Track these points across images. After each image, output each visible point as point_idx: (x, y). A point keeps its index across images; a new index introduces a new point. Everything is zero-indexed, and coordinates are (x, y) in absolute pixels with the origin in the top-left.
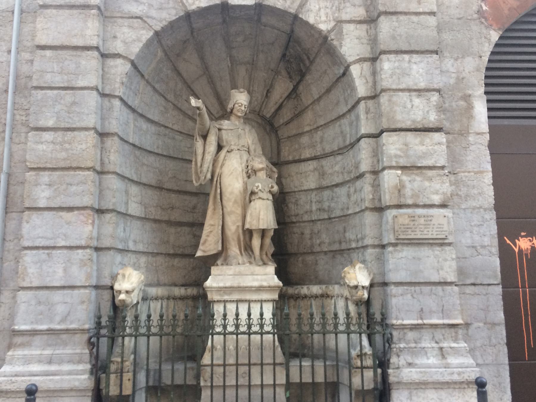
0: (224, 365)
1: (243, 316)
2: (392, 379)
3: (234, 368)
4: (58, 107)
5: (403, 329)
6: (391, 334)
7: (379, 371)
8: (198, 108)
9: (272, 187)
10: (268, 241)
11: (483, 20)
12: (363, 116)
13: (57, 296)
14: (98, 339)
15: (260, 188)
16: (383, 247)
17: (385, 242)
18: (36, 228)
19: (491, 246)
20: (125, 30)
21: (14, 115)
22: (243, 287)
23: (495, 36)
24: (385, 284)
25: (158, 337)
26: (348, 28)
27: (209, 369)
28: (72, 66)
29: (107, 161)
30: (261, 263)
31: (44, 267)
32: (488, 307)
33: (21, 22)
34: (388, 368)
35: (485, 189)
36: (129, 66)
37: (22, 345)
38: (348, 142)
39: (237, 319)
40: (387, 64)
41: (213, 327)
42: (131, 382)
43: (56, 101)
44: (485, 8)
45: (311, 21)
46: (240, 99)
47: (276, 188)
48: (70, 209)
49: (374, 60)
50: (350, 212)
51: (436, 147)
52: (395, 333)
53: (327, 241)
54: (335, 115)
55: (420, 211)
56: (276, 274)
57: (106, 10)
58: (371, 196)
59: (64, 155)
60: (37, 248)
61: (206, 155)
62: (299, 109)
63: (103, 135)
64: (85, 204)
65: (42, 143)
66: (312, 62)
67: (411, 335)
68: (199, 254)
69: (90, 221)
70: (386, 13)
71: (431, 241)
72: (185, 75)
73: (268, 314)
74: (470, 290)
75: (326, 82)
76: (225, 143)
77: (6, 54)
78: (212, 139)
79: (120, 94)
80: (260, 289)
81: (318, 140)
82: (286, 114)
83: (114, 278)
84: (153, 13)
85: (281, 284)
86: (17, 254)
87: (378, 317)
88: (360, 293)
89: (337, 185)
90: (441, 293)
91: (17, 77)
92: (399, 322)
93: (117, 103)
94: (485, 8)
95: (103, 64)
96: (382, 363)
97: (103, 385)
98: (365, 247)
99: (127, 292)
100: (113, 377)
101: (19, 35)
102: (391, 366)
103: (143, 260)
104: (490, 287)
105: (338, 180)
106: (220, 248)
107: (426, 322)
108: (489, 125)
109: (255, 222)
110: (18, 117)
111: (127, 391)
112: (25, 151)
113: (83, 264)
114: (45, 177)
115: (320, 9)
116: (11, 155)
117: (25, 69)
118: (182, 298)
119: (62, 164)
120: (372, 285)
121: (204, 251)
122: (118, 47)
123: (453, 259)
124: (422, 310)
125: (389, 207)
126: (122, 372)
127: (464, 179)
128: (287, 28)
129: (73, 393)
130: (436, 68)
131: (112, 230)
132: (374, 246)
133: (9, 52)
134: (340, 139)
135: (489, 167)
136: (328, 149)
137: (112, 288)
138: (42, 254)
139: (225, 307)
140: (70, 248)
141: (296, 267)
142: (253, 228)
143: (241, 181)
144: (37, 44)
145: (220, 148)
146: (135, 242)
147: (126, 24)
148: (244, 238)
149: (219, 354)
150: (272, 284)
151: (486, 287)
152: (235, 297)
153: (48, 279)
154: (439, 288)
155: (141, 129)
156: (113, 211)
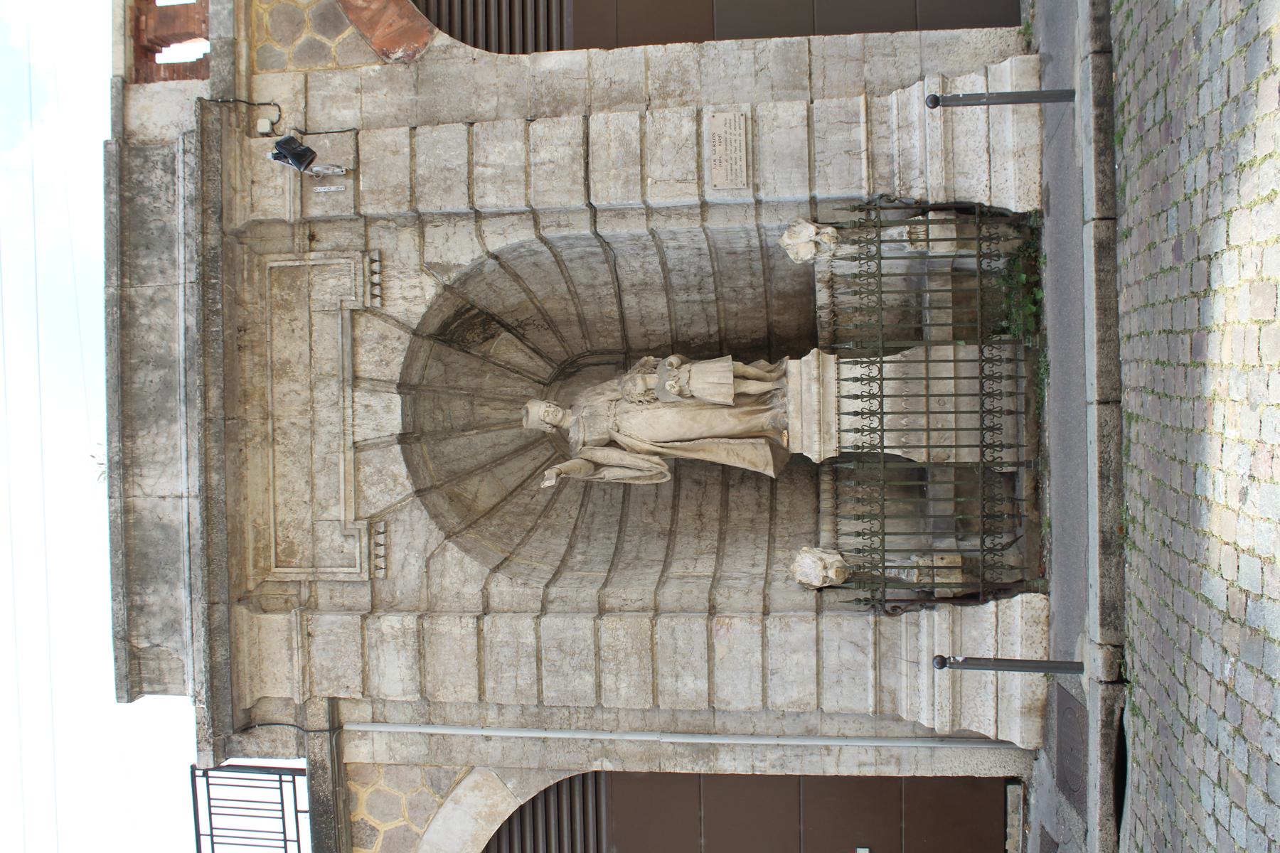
0: (928, 430)
1: (858, 405)
2: (941, 198)
3: (931, 416)
4: (567, 668)
5: (874, 179)
6: (881, 196)
7: (931, 215)
8: (558, 475)
9: (671, 365)
10: (750, 370)
11: (417, 56)
12: (565, 232)
13: (831, 659)
14: (887, 601)
15: (672, 383)
16: (758, 202)
17: (753, 201)
18: (738, 692)
19: (755, 49)
20: (446, 582)
21: (578, 729)
22: (820, 404)
23: (442, 39)
24: (813, 201)
25: (886, 521)
26: (431, 256)
27: (934, 451)
28: (507, 651)
29: (639, 604)
30: (784, 379)
31: (791, 678)
32: (841, 57)
33: (445, 723)
34: (927, 202)
35: (672, 56)
36: (500, 576)
37: (894, 701)
38: (599, 250)
39: (862, 413)
40: (490, 199)
41: (873, 447)
42: (945, 555)
43: (557, 672)
44: (399, 54)
45: (422, 309)
46: (539, 413)
47: (674, 359)
48: (710, 648)
49: (478, 216)
50: (705, 246)
51: (612, 128)
52: (880, 191)
53: (748, 278)
54: (554, 268)
55: (707, 151)
56: (799, 358)
57: (417, 609)
58: (684, 220)
59: (634, 660)
60: (764, 690)
61: (625, 463)
62: (542, 322)
63: (602, 611)
64: (703, 628)
65: (618, 689)
66: (473, 307)
67: (883, 169)
68: (770, 472)
69: (727, 620)
70: (413, 199)
71: (750, 137)
72: (494, 500)
73: (858, 371)
74: (818, 82)
75: (505, 284)
76: (606, 436)
77: (491, 743)
78: (602, 455)
79: (541, 586)
80: (821, 380)
81: (590, 292)
82: (548, 341)
83: (805, 587)
84: (419, 543)
85: (814, 351)
86: (772, 716)
87: (858, 216)
88: (825, 239)
89: (663, 264)
90: (824, 124)
91: (524, 727)
92: (865, 184)
93: (554, 591)
94: (399, 54)
95: (497, 612)
96: (922, 208)
97: (948, 592)
98: (759, 228)
99: (825, 568)
100: (938, 580)
101: (463, 725)
102: (924, 198)
103: (779, 554)
104: (814, 52)
105: (656, 260)
106: (763, 441)
107: (864, 147)
108: (575, 49)
109: (724, 390)
110: (581, 724)
111: (957, 560)
112: (629, 711)
113: (787, 627)
114: (667, 683)
115: (404, 298)
116: (634, 730)
117: (510, 715)
118: (836, 495)
119: (647, 661)
120: (815, 221)
121: (767, 464)
122: (472, 591)
123: (775, 106)
124: (847, 152)
125: (701, 195)
126: (933, 568)
127: (657, 86)
128: (427, 344)
129: (957, 630)
130: (494, 127)
131: (739, 592)
132: (758, 215)
133: (488, 738)
134: (591, 260)
135: (639, 50)
136: (608, 277)
137: (820, 590)
138: (774, 681)
139: (847, 431)
140: (765, 645)
141: (788, 320)
142: (732, 392)
143: (662, 411)
144: (476, 700)
145: (612, 443)
146: (753, 565)
147: (438, 580)
148: (746, 405)
149: (912, 439)
150: (814, 364)
151: (814, 58)
152: (832, 417)
153: (806, 672)
154: (817, 126)
155: (585, 562)
156: (710, 593)
